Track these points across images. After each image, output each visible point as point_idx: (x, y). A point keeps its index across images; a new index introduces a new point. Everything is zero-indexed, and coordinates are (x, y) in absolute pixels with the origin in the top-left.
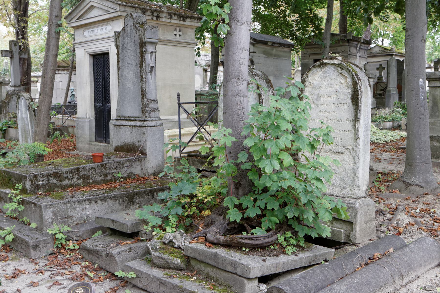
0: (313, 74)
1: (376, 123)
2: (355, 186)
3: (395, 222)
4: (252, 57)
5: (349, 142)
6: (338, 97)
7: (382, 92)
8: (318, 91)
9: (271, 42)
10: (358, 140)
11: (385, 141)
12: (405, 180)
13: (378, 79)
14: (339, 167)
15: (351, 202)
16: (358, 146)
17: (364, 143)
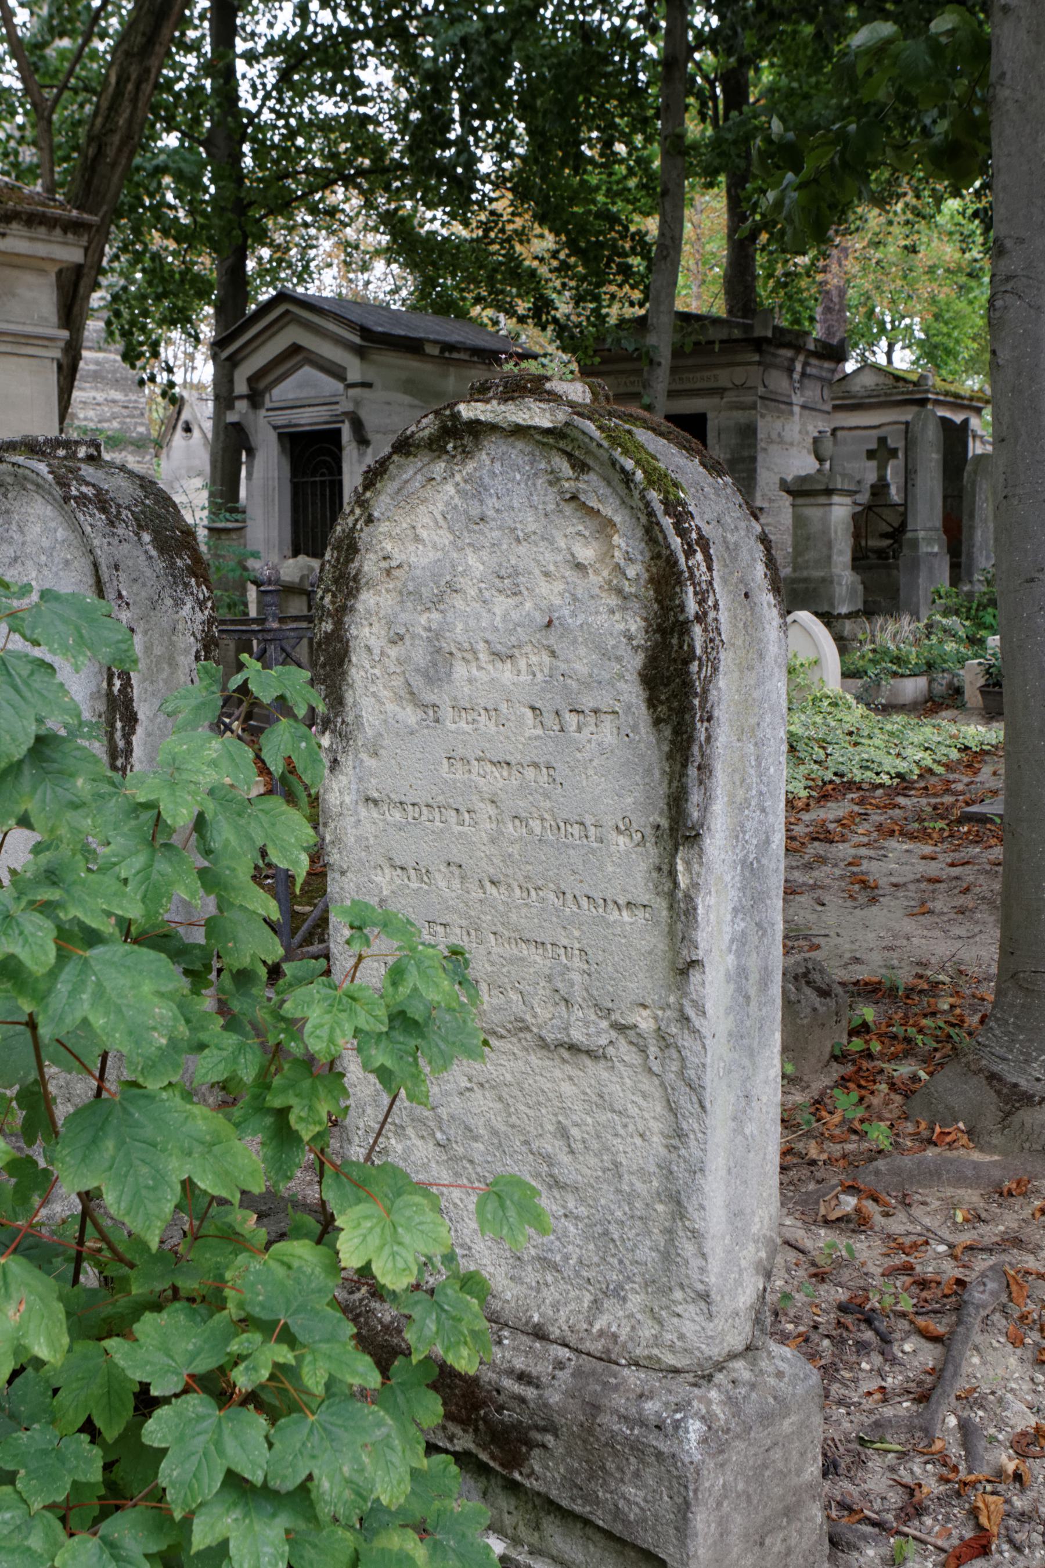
0: (405, 499)
1: (859, 682)
2: (678, 1295)
3: (952, 1421)
4: (357, 403)
5: (639, 982)
6: (563, 666)
7: (890, 542)
8: (436, 616)
9: (435, 342)
10: (695, 977)
11: (899, 775)
12: (998, 1068)
13: (874, 494)
14: (578, 1146)
15: (650, 1407)
16: (697, 1021)
17: (739, 989)
